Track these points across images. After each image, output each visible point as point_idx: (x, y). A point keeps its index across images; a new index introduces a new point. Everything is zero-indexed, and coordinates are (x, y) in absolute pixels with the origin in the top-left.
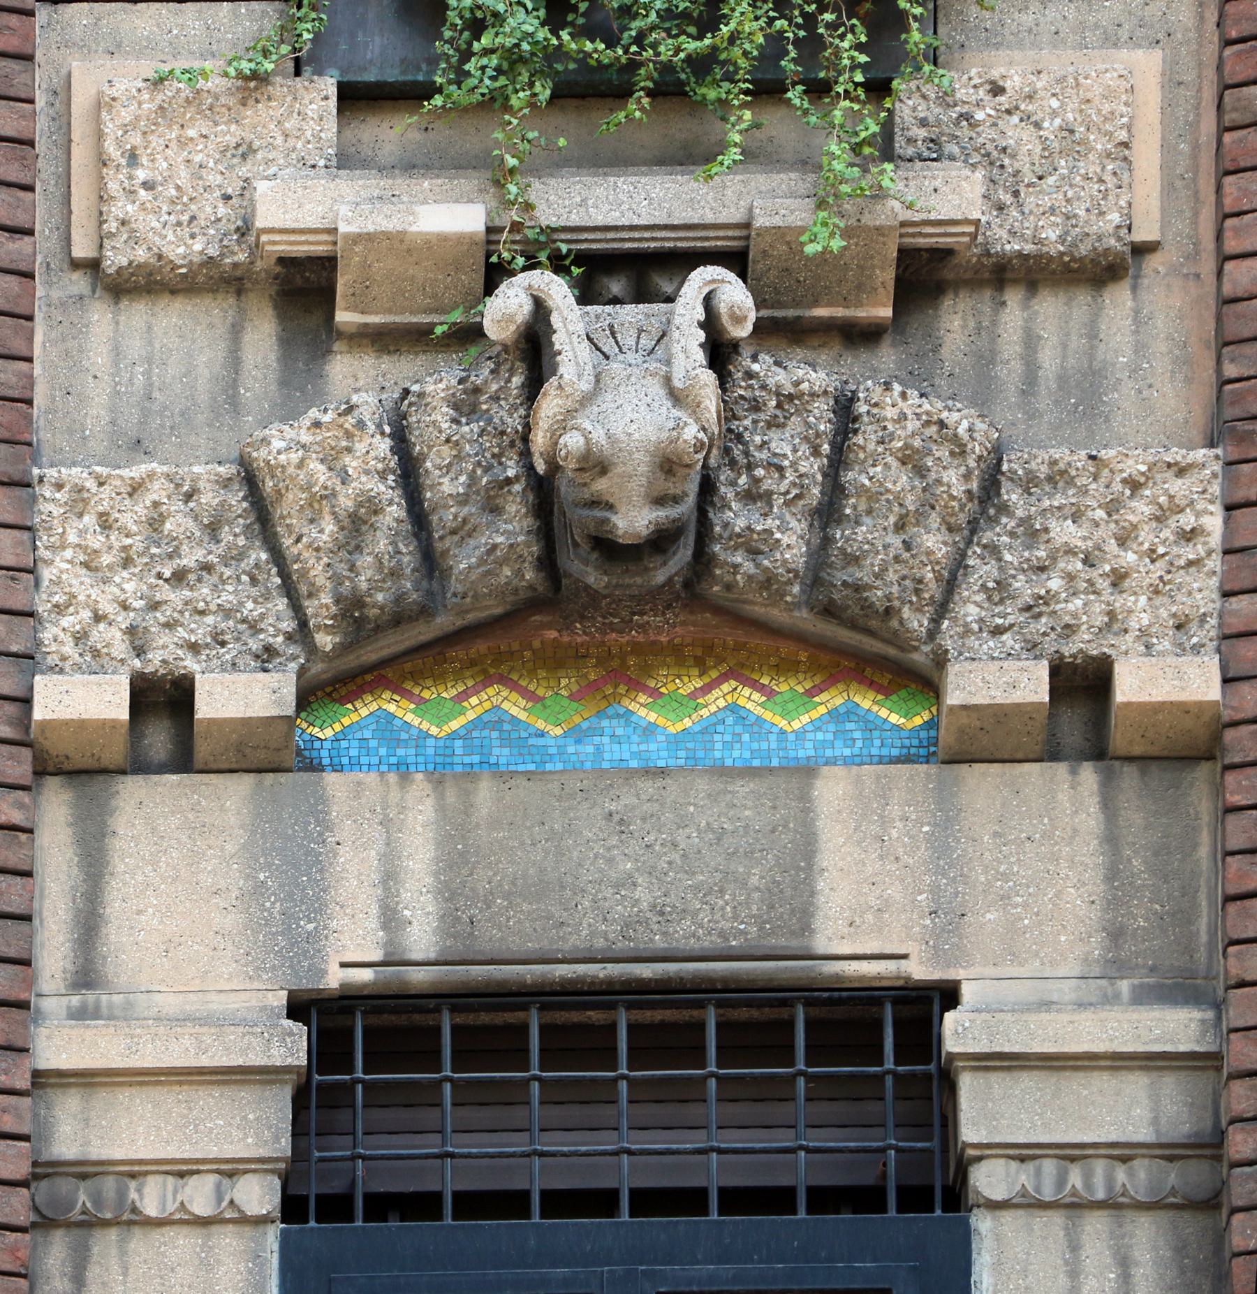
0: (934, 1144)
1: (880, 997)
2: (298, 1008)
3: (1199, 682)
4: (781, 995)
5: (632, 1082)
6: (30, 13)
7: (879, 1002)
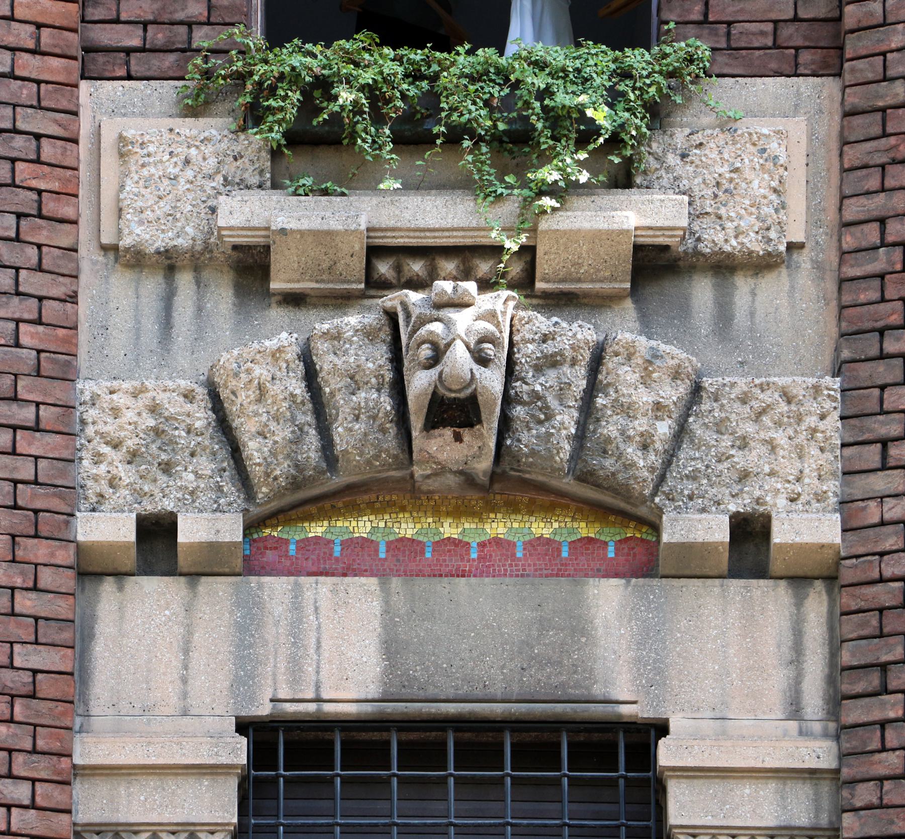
0: (651, 823)
1: (390, 727)
2: (243, 726)
3: (827, 530)
4: (556, 724)
5: (512, 777)
6: (76, 86)
7: (276, 730)
